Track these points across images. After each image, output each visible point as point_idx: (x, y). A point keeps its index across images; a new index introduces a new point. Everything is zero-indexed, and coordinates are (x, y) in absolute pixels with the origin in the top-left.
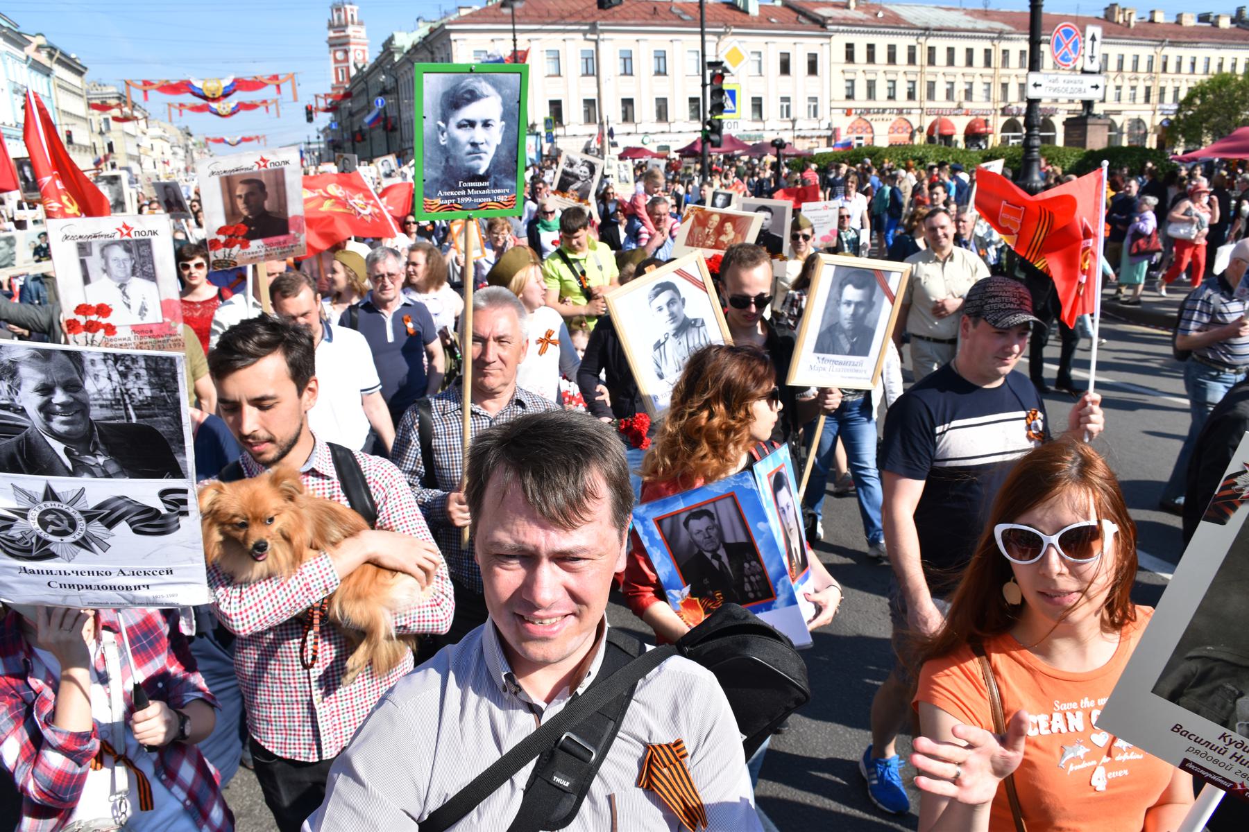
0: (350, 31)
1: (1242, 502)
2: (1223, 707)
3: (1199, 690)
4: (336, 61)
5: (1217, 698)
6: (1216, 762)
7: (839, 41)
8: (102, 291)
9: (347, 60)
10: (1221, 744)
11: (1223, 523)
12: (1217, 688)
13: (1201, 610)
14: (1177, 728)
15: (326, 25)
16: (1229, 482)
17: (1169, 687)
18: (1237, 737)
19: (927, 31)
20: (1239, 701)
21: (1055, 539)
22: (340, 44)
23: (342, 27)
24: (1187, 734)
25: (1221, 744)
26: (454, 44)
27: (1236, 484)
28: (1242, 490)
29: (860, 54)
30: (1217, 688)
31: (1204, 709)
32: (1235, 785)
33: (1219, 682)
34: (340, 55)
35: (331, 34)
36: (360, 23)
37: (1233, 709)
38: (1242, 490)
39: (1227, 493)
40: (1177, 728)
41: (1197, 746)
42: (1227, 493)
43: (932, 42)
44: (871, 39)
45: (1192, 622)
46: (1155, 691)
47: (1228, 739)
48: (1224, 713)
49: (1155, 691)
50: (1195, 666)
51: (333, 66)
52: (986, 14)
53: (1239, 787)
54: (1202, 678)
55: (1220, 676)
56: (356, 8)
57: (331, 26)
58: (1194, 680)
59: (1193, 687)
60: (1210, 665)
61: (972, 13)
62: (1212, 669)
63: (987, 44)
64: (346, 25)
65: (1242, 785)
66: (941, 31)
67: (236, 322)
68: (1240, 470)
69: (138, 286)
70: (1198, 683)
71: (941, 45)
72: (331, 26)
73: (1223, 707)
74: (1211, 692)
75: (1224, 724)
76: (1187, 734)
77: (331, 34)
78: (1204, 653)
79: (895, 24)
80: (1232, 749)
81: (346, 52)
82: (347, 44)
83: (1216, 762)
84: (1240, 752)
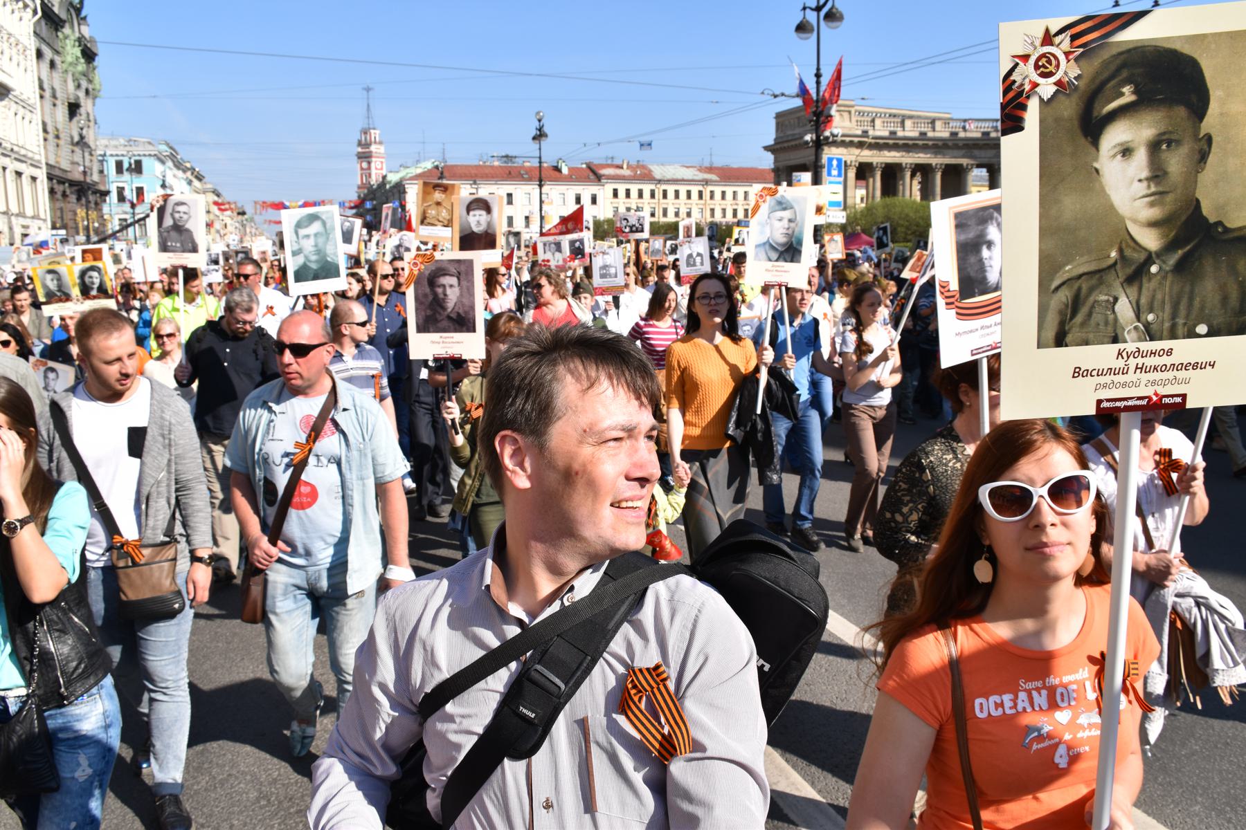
0: (373, 148)
1: (1028, 97)
2: (1106, 323)
3: (1079, 318)
4: (362, 169)
5: (1097, 317)
6: (1124, 385)
7: (609, 188)
8: (548, 256)
9: (369, 168)
10: (1120, 363)
11: (1022, 129)
12: (1093, 307)
13: (1044, 232)
14: (1077, 373)
15: (356, 142)
16: (1008, 82)
17: (1050, 334)
18: (1131, 346)
19: (660, 181)
20: (1117, 307)
21: (1044, 491)
22: (365, 157)
23: (368, 145)
24: (1089, 373)
25: (1120, 363)
26: (450, 163)
27: (1014, 82)
28: (1022, 85)
29: (622, 193)
30: (1093, 307)
31: (1091, 336)
32: (1150, 398)
33: (1092, 299)
34: (365, 165)
35: (360, 150)
36: (380, 143)
37: (1116, 320)
38: (1022, 85)
39: (1011, 95)
40: (1077, 373)
41: (1102, 380)
42: (1011, 95)
43: (664, 187)
44: (628, 186)
45: (1041, 251)
46: (1040, 345)
47: (1124, 354)
48: (1110, 329)
49: (1040, 345)
50: (1064, 295)
51: (359, 172)
52: (710, 170)
53: (1155, 398)
54: (1076, 304)
55: (1091, 290)
56: (377, 132)
57: (360, 144)
58: (1069, 311)
59: (1071, 319)
60: (1076, 286)
61: (701, 170)
62: (1079, 289)
63: (701, 188)
64: (370, 144)
65: (1156, 394)
66: (669, 181)
67: (346, 776)
68: (1011, 65)
69: (558, 255)
70: (1075, 312)
71: (671, 189)
72: (360, 144)
73: (1106, 323)
74: (1090, 315)
75: (1115, 340)
76: (1089, 373)
77: (360, 150)
78: (1066, 276)
79: (647, 177)
80: (1132, 362)
81: (369, 163)
82: (371, 157)
83: (1124, 385)
84: (1140, 361)
